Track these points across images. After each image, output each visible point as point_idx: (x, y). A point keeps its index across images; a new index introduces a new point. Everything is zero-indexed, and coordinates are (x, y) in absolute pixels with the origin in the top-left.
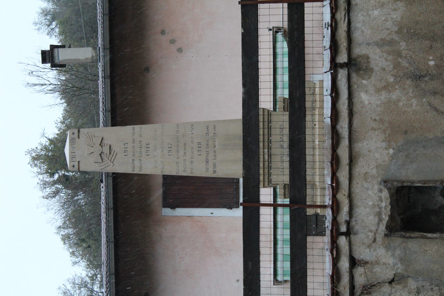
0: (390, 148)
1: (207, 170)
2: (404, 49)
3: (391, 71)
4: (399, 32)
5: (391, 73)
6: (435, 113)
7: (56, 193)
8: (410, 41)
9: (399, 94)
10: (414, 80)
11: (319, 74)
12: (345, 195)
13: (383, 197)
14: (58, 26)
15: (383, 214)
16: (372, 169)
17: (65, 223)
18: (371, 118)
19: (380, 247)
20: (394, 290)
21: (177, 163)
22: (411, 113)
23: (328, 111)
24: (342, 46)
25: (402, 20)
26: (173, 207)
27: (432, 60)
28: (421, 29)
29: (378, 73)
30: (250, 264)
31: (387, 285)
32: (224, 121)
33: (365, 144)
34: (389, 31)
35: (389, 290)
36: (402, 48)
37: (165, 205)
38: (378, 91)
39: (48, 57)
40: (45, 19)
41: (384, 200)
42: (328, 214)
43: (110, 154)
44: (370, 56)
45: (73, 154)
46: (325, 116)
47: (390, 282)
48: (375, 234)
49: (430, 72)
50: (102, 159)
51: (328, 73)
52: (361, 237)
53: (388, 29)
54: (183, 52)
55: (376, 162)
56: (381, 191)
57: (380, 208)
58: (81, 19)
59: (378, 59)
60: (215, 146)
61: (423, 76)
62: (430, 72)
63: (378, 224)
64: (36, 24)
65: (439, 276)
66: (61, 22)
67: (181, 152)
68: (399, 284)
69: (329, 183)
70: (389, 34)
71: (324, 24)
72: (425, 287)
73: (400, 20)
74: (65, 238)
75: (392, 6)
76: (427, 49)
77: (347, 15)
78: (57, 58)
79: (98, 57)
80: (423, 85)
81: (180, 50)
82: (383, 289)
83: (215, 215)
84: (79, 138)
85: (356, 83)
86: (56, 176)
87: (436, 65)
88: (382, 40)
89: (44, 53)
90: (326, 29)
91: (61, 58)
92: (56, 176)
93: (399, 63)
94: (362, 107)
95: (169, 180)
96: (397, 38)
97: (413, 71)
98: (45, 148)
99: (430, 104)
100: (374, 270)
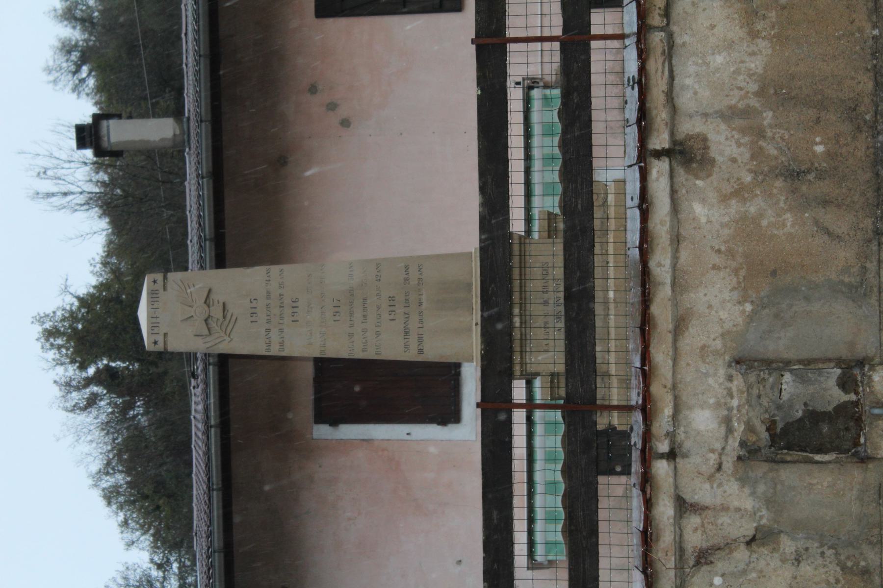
0: (745, 301)
1: (407, 347)
2: (771, 126)
3: (746, 164)
4: (761, 93)
5: (747, 167)
6: (826, 237)
7: (92, 401)
8: (781, 109)
9: (762, 204)
10: (788, 180)
11: (613, 165)
12: (665, 387)
13: (734, 389)
14: (93, 73)
15: (735, 419)
16: (714, 340)
17: (108, 464)
18: (712, 248)
19: (729, 481)
20: (755, 556)
21: (351, 335)
22: (783, 238)
23: (634, 237)
24: (659, 119)
25: (766, 71)
26: (335, 422)
27: (820, 143)
28: (800, 88)
29: (724, 167)
30: (495, 514)
31: (743, 547)
32: (438, 257)
33: (701, 295)
34: (742, 93)
35: (747, 557)
36: (765, 123)
37: (321, 417)
38: (724, 199)
39: (87, 136)
40: (67, 61)
41: (735, 394)
42: (637, 421)
43: (224, 317)
44: (709, 136)
45: (154, 320)
46: (629, 245)
47: (749, 543)
48: (720, 455)
49: (816, 165)
50: (209, 329)
51: (633, 167)
52: (697, 462)
53: (740, 89)
54: (352, 126)
55: (722, 327)
56: (730, 378)
57: (730, 409)
58: (141, 60)
59: (725, 144)
60: (420, 304)
61: (804, 172)
62: (816, 165)
63: (726, 438)
64: (49, 70)
65: (835, 531)
66: (99, 67)
67: (358, 315)
68: (763, 545)
69: (638, 365)
70: (741, 98)
71: (626, 79)
72: (810, 551)
73: (762, 72)
74: (110, 496)
75: (748, 46)
76: (811, 124)
77: (667, 63)
78: (106, 139)
79: (186, 137)
80: (804, 188)
81: (345, 123)
82: (735, 554)
83: (413, 437)
84: (165, 289)
85: (683, 185)
86: (91, 371)
87: (828, 154)
88: (731, 107)
89: (81, 130)
90: (630, 88)
91: (113, 139)
92: (91, 371)
93: (761, 148)
94: (695, 228)
95: (327, 369)
96: (757, 105)
97: (786, 164)
98: (72, 316)
99: (816, 222)
100: (720, 521)
